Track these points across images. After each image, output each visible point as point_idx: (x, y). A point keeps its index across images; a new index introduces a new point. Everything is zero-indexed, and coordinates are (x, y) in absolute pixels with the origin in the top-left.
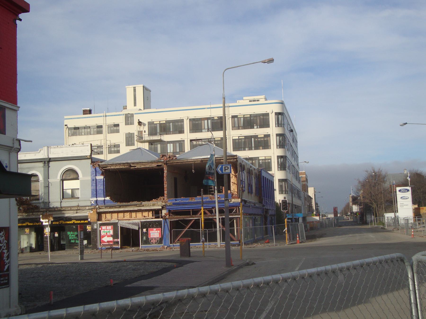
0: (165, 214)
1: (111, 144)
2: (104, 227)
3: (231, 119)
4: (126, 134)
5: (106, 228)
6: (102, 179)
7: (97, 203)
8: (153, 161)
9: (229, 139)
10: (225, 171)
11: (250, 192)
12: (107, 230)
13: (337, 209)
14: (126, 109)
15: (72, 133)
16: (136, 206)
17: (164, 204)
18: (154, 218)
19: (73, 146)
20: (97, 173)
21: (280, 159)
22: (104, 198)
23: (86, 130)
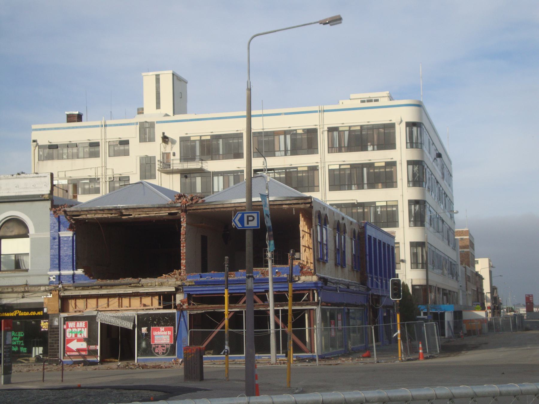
0: (181, 301)
1: (113, 175)
2: (71, 324)
3: (326, 133)
4: (142, 159)
5: (76, 326)
6: (69, 237)
7: (59, 279)
8: (161, 206)
9: (322, 169)
10: (248, 224)
11: (340, 263)
12: (77, 328)
13: (533, 299)
14: (143, 113)
15: (45, 155)
16: (129, 287)
17: (179, 283)
18: (161, 308)
19: (18, 176)
20: (61, 226)
21: (413, 206)
22: (73, 270)
23: (70, 150)
